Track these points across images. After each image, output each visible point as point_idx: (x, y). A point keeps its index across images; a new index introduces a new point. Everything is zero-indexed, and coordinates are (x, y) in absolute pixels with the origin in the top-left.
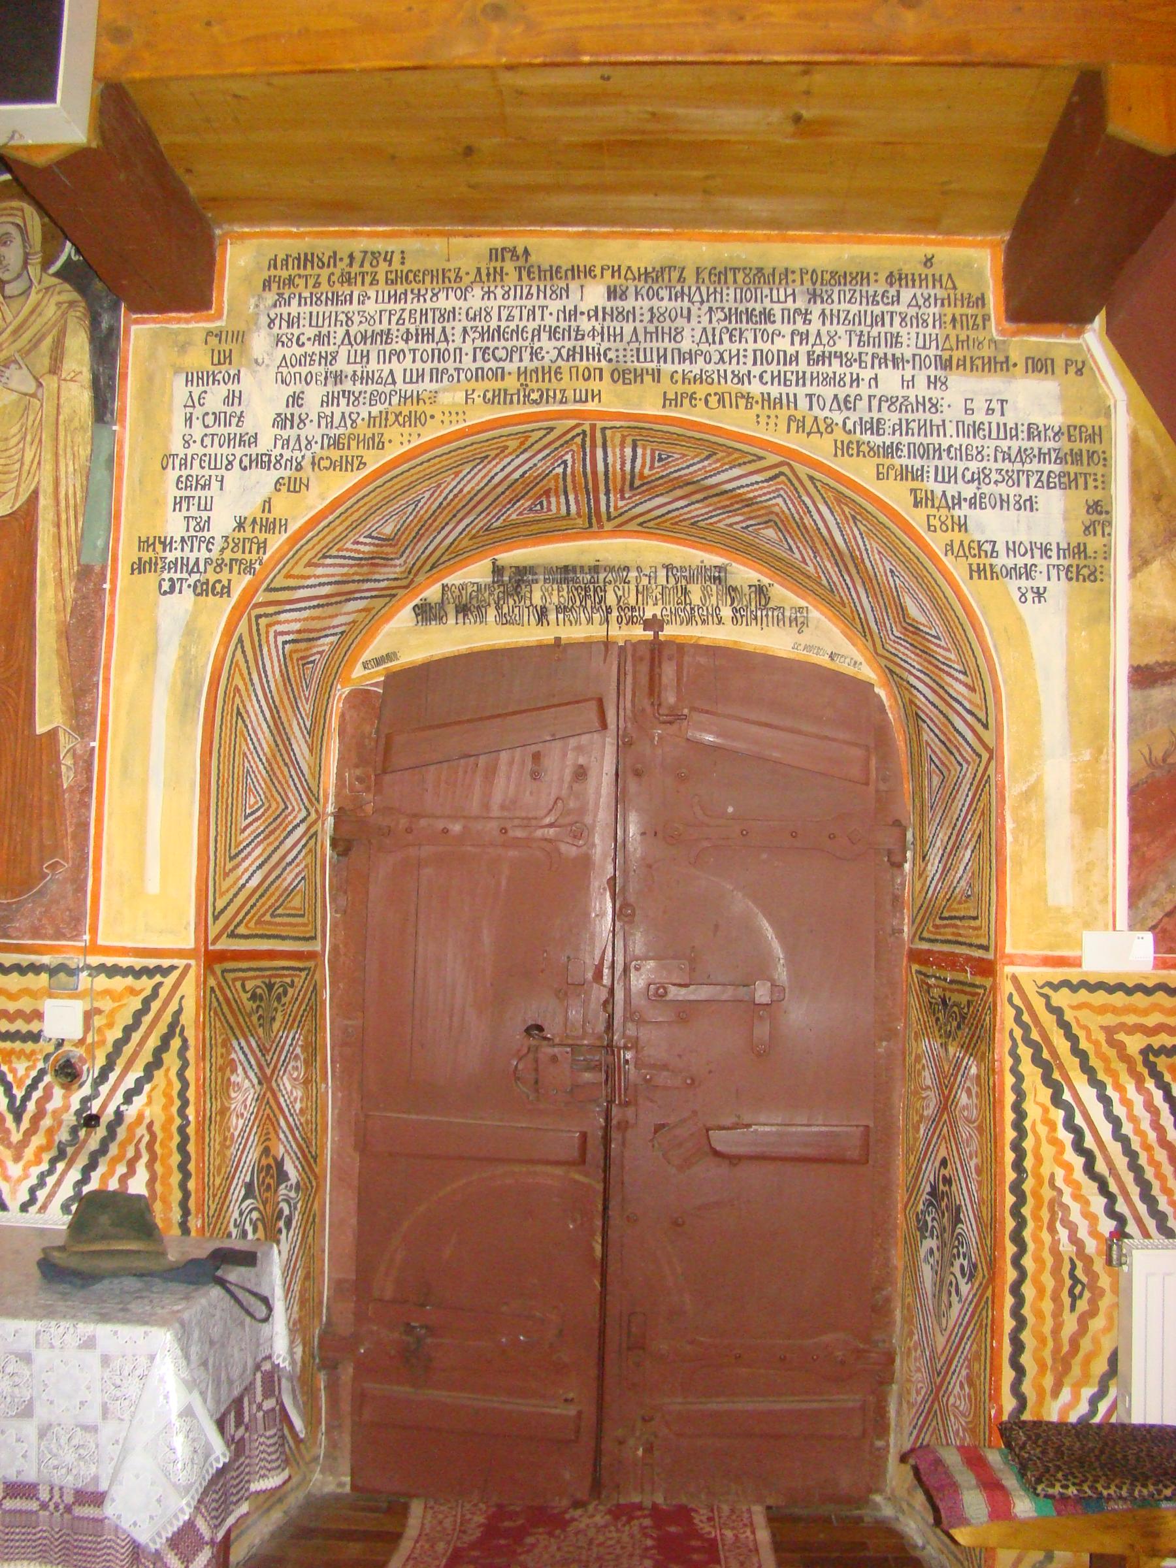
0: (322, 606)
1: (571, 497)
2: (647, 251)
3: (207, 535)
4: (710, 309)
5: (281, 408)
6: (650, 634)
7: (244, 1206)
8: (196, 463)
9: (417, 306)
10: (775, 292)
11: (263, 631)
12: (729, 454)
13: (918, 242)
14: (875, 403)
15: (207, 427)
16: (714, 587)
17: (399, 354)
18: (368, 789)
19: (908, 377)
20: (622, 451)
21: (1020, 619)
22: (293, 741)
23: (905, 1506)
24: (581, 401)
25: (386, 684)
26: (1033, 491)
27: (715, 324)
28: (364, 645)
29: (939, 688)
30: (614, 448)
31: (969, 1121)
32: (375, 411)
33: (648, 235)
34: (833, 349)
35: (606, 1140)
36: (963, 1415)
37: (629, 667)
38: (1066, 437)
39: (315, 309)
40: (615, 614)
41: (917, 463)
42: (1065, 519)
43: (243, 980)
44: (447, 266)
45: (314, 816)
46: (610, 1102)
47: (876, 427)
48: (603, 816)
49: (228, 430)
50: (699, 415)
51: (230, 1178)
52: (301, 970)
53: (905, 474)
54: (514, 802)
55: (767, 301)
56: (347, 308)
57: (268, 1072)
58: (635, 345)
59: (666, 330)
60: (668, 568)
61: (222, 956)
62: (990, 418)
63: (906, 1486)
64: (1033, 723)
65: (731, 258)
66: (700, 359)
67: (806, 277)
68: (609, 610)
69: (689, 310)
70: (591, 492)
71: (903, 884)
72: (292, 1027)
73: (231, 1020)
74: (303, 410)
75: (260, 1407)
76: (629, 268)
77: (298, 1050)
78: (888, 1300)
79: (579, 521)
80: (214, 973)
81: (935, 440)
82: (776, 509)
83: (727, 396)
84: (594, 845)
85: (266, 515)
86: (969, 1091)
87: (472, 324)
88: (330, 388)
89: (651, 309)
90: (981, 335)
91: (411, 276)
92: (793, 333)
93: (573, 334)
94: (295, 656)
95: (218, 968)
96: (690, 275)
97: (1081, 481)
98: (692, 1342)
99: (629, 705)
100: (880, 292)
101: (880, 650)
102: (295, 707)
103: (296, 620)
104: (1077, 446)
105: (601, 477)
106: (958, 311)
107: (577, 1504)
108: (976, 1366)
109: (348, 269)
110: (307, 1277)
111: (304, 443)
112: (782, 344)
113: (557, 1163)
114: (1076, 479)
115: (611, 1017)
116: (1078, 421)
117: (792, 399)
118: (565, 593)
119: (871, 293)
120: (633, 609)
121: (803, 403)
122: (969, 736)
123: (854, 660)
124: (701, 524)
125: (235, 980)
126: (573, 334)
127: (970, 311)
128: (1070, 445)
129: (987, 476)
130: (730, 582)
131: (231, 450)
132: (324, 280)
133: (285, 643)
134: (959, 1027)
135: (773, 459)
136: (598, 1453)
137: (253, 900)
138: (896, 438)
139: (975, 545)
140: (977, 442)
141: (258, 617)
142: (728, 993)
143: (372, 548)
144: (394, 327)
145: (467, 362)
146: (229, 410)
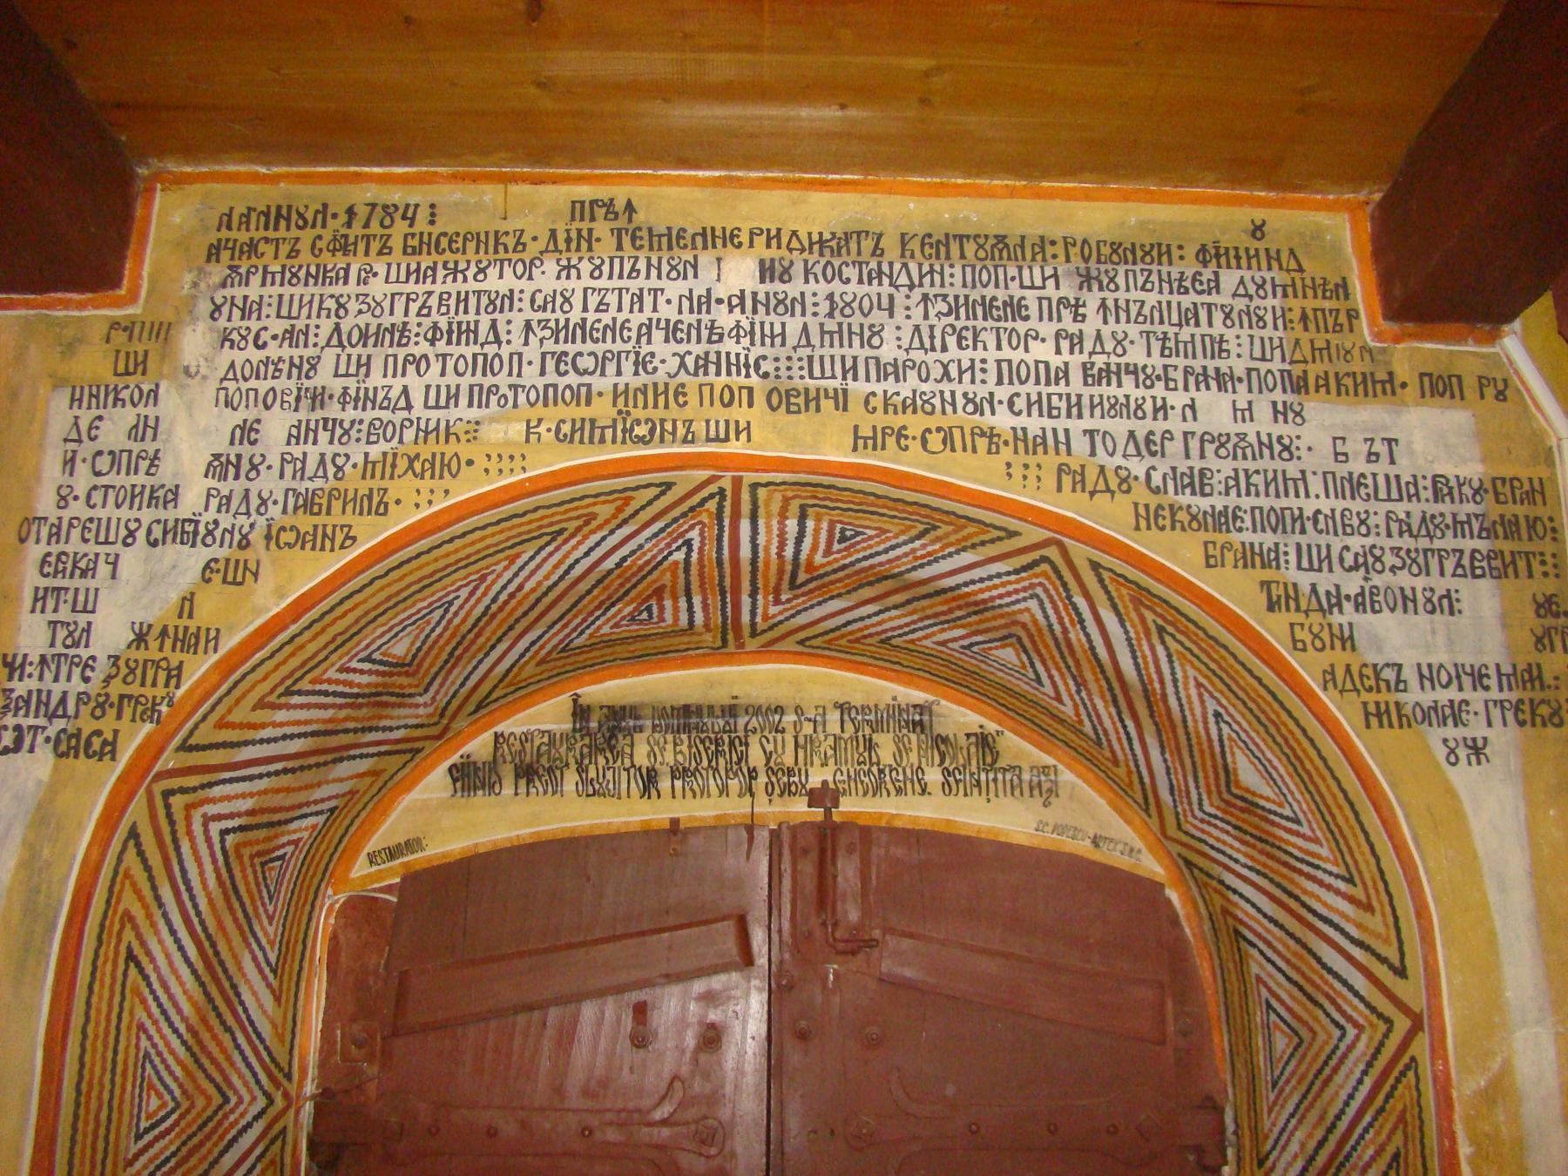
0: (293, 771)
1: (697, 600)
2: (822, 209)
3: (84, 653)
4: (925, 298)
5: (222, 446)
8: (76, 534)
9: (450, 287)
10: (1026, 272)
11: (179, 816)
13: (1238, 202)
14: (1194, 444)
16: (913, 737)
17: (418, 362)
18: (370, 1058)
19: (1242, 405)
21: (1450, 791)
22: (243, 989)
24: (717, 439)
26: (1450, 583)
27: (933, 320)
29: (1290, 899)
30: (769, 517)
32: (375, 452)
33: (825, 185)
34: (1123, 360)
37: (786, 865)
38: (1491, 495)
39: (287, 290)
40: (762, 779)
42: (1505, 626)
44: (503, 227)
45: (280, 1102)
47: (1198, 483)
49: (133, 479)
50: (912, 463)
53: (1249, 557)
54: (604, 1083)
55: (1014, 285)
56: (337, 289)
58: (804, 352)
59: (856, 329)
60: (842, 707)
62: (1373, 468)
64: (1487, 969)
65: (954, 221)
66: (912, 375)
67: (1072, 251)
69: (891, 297)
76: (794, 233)
79: (708, 637)
81: (1292, 502)
82: (1025, 618)
83: (957, 434)
85: (185, 622)
87: (540, 315)
88: (303, 415)
89: (830, 297)
90: (1347, 341)
91: (444, 242)
92: (1057, 335)
93: (705, 333)
94: (246, 852)
96: (890, 244)
97: (1521, 564)
99: (786, 925)
100: (1189, 273)
102: (247, 931)
103: (244, 796)
104: (1511, 509)
105: (746, 568)
106: (1310, 304)
109: (344, 231)
111: (255, 502)
112: (1042, 351)
114: (1513, 562)
116: (1507, 472)
117: (1062, 438)
118: (684, 748)
119: (1175, 276)
120: (790, 772)
121: (1080, 445)
122: (1359, 981)
124: (894, 642)
126: (705, 333)
127: (1327, 305)
128: (1499, 509)
129: (1378, 559)
131: (135, 514)
132: (305, 246)
135: (1036, 534)
139: (1368, 671)
140: (1357, 506)
141: (167, 794)
143: (373, 679)
144: (413, 319)
145: (530, 375)
146: (136, 447)
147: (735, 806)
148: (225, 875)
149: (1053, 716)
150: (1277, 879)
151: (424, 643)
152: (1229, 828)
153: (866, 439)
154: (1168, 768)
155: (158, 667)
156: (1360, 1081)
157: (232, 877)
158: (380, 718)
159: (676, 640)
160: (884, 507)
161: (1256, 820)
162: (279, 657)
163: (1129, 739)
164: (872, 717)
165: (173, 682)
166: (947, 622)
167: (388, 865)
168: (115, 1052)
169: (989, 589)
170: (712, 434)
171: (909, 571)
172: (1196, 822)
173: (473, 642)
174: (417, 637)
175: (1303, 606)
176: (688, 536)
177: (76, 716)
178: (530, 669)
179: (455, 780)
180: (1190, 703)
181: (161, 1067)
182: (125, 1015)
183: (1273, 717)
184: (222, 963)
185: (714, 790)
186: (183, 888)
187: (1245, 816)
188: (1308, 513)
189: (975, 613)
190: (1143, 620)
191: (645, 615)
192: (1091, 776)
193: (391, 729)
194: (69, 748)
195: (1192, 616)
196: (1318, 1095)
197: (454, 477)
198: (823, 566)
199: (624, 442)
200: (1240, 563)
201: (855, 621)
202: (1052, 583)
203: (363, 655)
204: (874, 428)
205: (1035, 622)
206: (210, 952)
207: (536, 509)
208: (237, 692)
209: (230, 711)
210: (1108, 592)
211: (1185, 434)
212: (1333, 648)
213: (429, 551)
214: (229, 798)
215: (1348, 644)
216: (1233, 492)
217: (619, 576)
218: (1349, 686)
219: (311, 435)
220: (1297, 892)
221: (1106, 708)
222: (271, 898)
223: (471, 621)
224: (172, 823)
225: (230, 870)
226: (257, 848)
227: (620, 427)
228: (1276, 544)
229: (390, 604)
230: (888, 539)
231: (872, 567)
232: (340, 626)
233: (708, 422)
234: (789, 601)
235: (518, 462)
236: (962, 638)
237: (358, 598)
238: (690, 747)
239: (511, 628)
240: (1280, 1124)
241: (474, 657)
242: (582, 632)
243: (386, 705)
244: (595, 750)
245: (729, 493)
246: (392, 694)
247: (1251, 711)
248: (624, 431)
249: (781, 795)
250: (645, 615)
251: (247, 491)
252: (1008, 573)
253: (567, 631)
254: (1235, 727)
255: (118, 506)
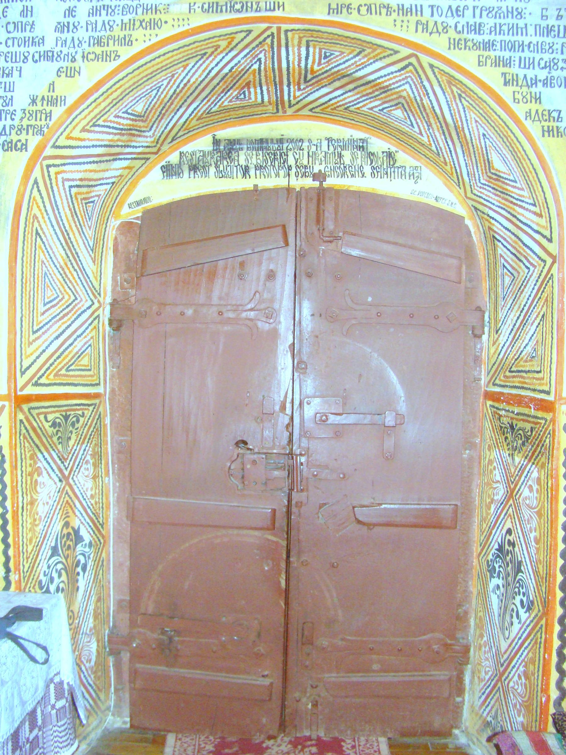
0: (97, 162)
1: (265, 88)
3: (11, 109)
5: (62, 19)
6: (317, 184)
7: (50, 562)
11: (53, 177)
12: (375, 50)
14: (478, 12)
15: (9, 32)
16: (359, 153)
18: (132, 287)
20: (299, 50)
23: (475, 740)
24: (270, 10)
25: (142, 218)
28: (129, 192)
29: (513, 218)
30: (293, 46)
31: (530, 507)
32: (126, 19)
35: (289, 513)
36: (520, 696)
40: (294, 170)
41: (507, 54)
43: (46, 414)
46: (291, 490)
47: (478, 29)
48: (287, 303)
49: (24, 34)
50: (353, 19)
51: (39, 546)
52: (89, 405)
57: (67, 473)
60: (329, 140)
61: (28, 399)
63: (477, 727)
68: (290, 168)
70: (278, 85)
71: (481, 349)
72: (83, 443)
73: (37, 442)
74: (76, 20)
75: (53, 707)
77: (88, 457)
78: (466, 613)
79: (270, 107)
80: (22, 410)
81: (519, 38)
82: (404, 94)
84: (280, 322)
85: (51, 94)
86: (530, 488)
94: (79, 197)
95: (25, 407)
98: (343, 639)
101: (469, 195)
107: (270, 738)
108: (531, 667)
110: (99, 600)
111: (77, 42)
113: (256, 529)
115: (291, 434)
117: (419, 9)
118: (261, 157)
120: (306, 167)
123: (451, 202)
124: (351, 109)
125: (38, 414)
129: (555, 64)
130: (370, 150)
133: (71, 187)
134: (523, 444)
135: (405, 52)
136: (283, 707)
137: (52, 361)
138: (492, 37)
139: (546, 113)
140: (549, 40)
141: (48, 166)
142: (368, 419)
146: (24, 20)
147: (281, 182)
148: (71, 206)
149: (419, 143)
150: (509, 210)
151: (149, 106)
152: (490, 189)
153: (334, 10)
154: (466, 164)
155: (42, 113)
156: (533, 289)
157: (74, 207)
158: (132, 141)
159: (256, 109)
160: (342, 40)
161: (500, 184)
162: (90, 108)
163: (451, 151)
164: (342, 144)
165: (48, 118)
166: (372, 98)
167: (137, 208)
168: (34, 270)
169: (389, 80)
170: (268, 8)
171: (354, 72)
172: (478, 189)
173: (170, 107)
174: (146, 103)
175: (520, 84)
176: (259, 57)
177: (10, 134)
178: (194, 122)
179: (163, 172)
180: (473, 131)
181: (51, 280)
182: (37, 256)
183: (505, 133)
184: (71, 242)
185: (273, 175)
186: (55, 208)
187: (496, 182)
188: (526, 43)
189: (384, 92)
190: (452, 92)
191: (242, 96)
192: (436, 171)
193: (136, 147)
194: (8, 147)
195: (472, 88)
196: (519, 298)
197: (160, 28)
198: (318, 71)
199: (230, 11)
200: (494, 65)
201: (333, 98)
202: (415, 76)
203: (124, 110)
204: (337, 5)
205: (409, 95)
206: (67, 237)
207: (194, 43)
208: (74, 123)
209: (71, 132)
210: (437, 79)
211: (474, 7)
212: (531, 102)
213: (150, 61)
214: (72, 172)
215: (538, 101)
216: (493, 33)
217: (231, 76)
218: (537, 118)
219: (98, 12)
220: (516, 214)
221: (440, 136)
222: (90, 219)
223: (168, 97)
224: (50, 180)
225: (73, 204)
226: (83, 196)
227: (229, 5)
228: (510, 57)
229: (135, 86)
230: (345, 56)
231: (339, 71)
232: (115, 95)
233: (266, 3)
234: (304, 89)
235: (186, 22)
236: (379, 105)
237: (121, 83)
238: (263, 156)
239: (186, 101)
240: (505, 314)
241: (170, 114)
242: (216, 104)
243: (134, 135)
244: (223, 158)
245: (275, 35)
246: (137, 130)
247: (496, 131)
248: (230, 7)
249: (302, 177)
250: (242, 96)
251: (73, 38)
252: (396, 72)
253: (209, 103)
254: (491, 140)
255: (19, 46)
